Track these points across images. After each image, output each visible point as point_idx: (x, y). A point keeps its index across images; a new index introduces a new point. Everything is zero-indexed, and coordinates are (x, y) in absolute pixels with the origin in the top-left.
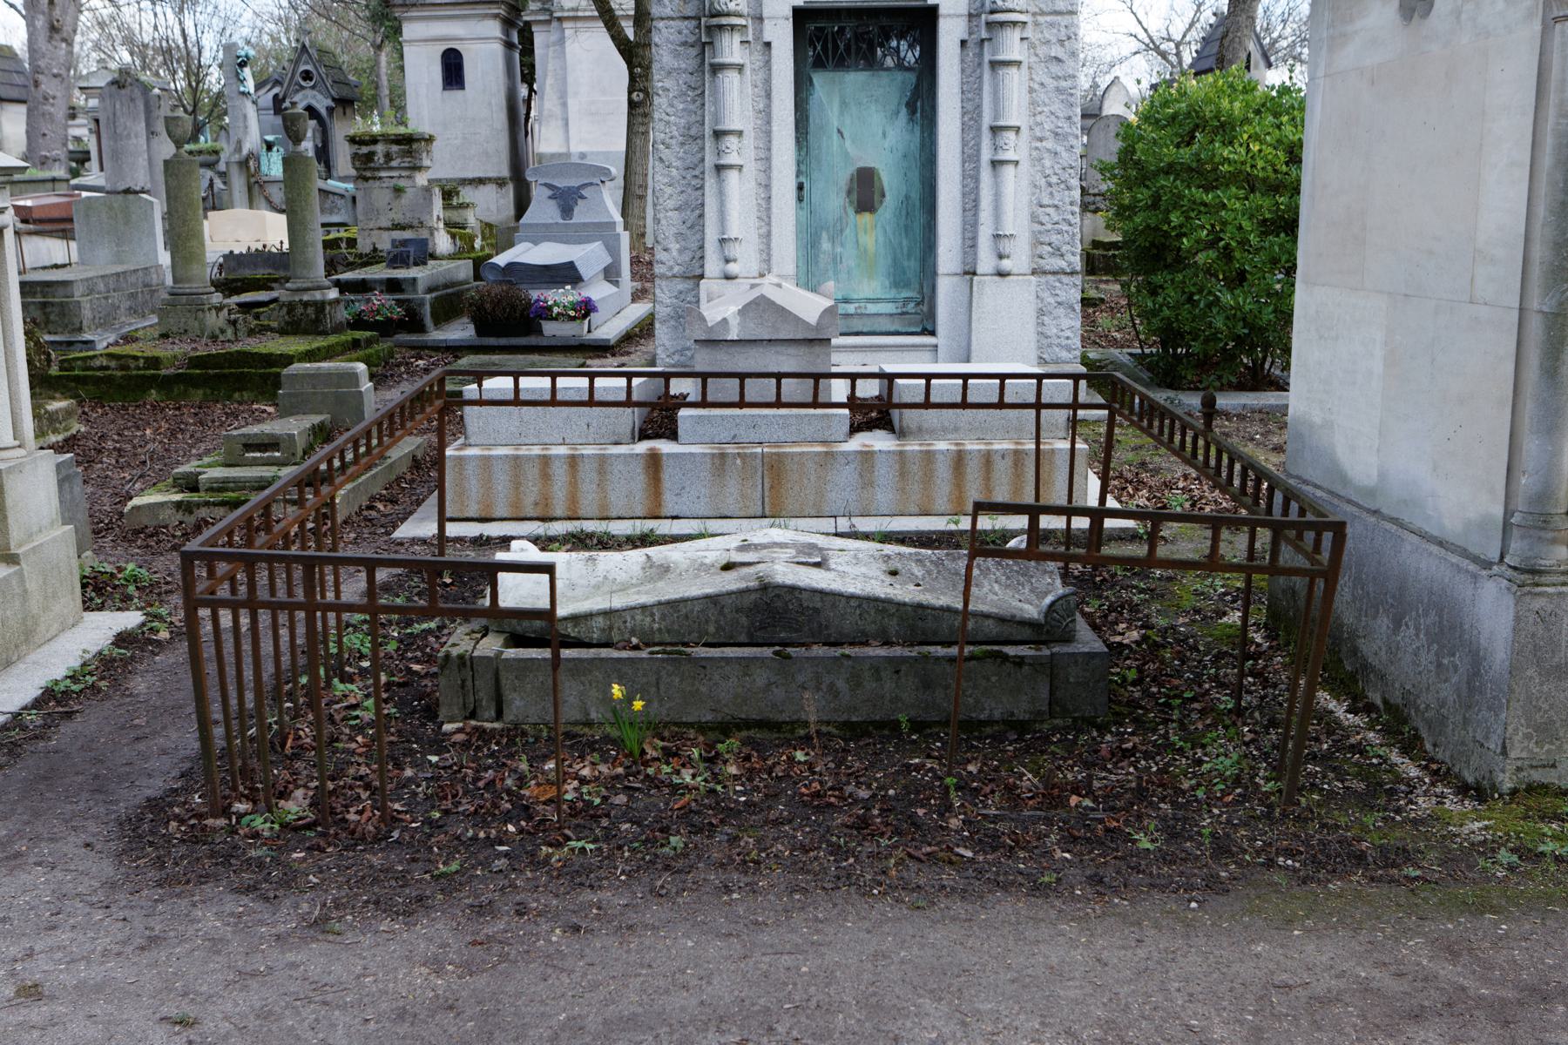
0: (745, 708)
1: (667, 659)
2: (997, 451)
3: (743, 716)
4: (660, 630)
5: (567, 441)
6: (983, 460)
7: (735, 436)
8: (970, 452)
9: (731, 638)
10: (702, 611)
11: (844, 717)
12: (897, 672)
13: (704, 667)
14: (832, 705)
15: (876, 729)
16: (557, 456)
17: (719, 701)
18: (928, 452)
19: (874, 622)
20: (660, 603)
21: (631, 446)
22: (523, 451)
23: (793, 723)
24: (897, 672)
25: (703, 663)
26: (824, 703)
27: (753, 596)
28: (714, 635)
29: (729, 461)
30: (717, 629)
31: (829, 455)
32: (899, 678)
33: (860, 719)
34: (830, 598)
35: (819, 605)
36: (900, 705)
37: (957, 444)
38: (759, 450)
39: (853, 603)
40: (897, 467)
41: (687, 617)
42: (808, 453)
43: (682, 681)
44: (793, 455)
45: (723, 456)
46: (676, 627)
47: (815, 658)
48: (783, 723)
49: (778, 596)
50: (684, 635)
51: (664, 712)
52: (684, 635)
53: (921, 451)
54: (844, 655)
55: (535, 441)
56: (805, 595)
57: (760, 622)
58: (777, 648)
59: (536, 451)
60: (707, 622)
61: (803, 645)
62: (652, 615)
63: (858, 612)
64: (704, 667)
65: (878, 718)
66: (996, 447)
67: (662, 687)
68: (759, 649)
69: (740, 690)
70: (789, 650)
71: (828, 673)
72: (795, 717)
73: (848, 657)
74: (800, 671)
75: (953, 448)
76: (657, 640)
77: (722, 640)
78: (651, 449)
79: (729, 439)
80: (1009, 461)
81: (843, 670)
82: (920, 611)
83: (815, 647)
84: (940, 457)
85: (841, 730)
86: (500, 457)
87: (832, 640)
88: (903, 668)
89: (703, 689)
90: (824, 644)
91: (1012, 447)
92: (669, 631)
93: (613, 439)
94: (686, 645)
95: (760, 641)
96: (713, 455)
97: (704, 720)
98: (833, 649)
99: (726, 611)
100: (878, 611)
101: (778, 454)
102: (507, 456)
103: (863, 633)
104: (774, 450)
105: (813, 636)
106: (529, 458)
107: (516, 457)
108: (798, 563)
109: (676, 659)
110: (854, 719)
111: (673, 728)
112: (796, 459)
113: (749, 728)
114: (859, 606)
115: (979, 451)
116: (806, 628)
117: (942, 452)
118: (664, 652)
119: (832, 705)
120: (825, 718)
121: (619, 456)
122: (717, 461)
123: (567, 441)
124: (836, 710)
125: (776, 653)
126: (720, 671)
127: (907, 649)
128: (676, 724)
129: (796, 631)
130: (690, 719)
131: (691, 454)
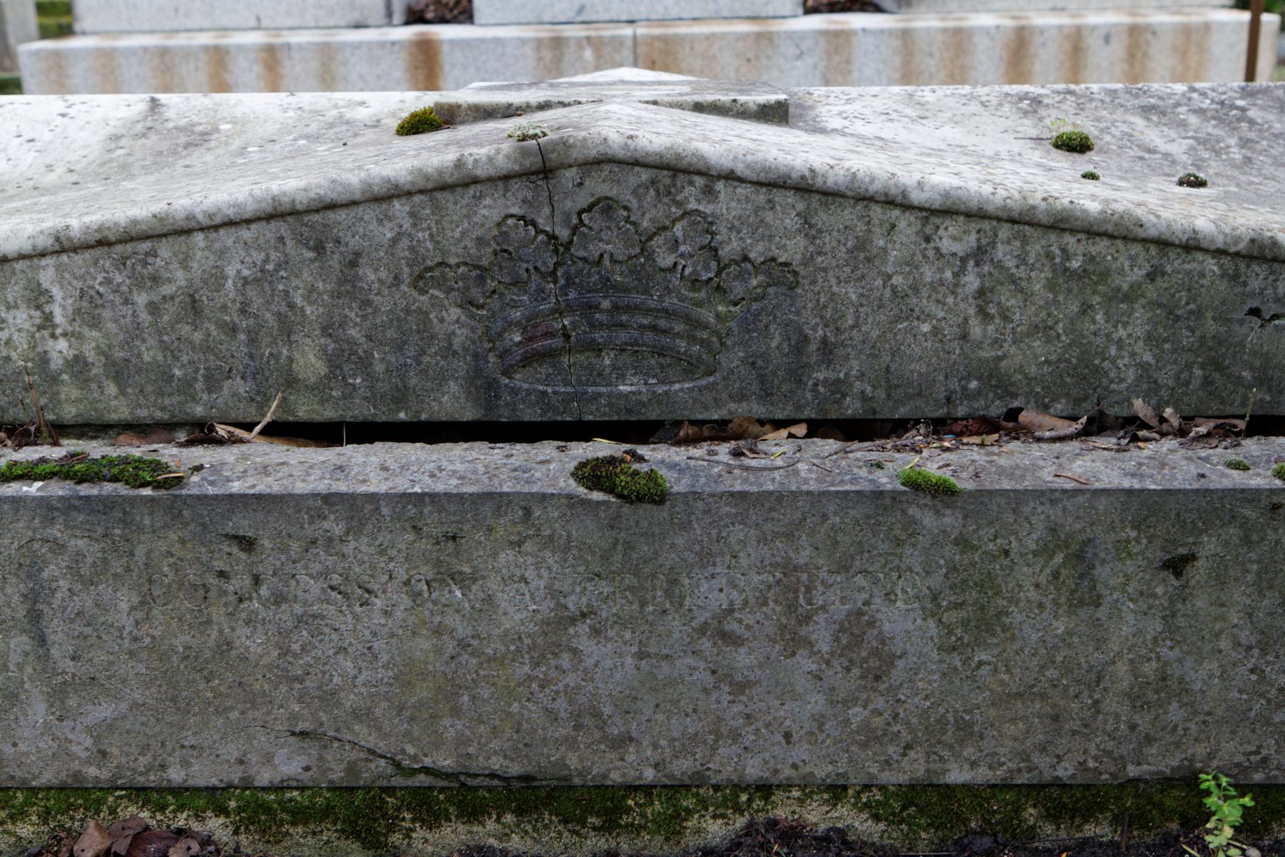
0: (451, 727)
1: (68, 506)
2: (1094, 28)
3: (446, 762)
4: (78, 365)
5: (265, 23)
6: (1067, 47)
7: (581, 9)
8: (1042, 31)
9: (400, 399)
10: (262, 278)
11: (914, 767)
12: (1177, 565)
13: (247, 544)
14: (857, 714)
15: (1054, 815)
16: (241, 48)
17: (329, 698)
18: (958, 32)
19: (1043, 329)
20: (63, 246)
21: (386, 30)
22: (180, 41)
23: (675, 789)
24: (1177, 565)
25: (242, 524)
26: (817, 703)
27: (492, 209)
28: (320, 389)
29: (570, 54)
30: (334, 363)
31: (765, 38)
32: (1182, 595)
33: (982, 775)
34: (849, 214)
35: (793, 249)
36: (1175, 712)
37: (1014, 18)
38: (628, 31)
39: (954, 238)
40: (897, 61)
41: (193, 307)
42: (723, 35)
43: (146, 603)
44: (692, 39)
45: (557, 43)
46: (149, 353)
47: (780, 498)
48: (633, 789)
49: (605, 206)
50: (186, 387)
51: (82, 744)
52: (186, 387)
53: (945, 31)
54: (917, 485)
55: (206, 23)
56: (728, 204)
57: (529, 327)
58: (602, 448)
59: (205, 39)
60: (287, 329)
61: (719, 431)
62: (38, 298)
63: (972, 281)
64: (247, 544)
65: (1065, 771)
66: (1093, 19)
67: (57, 630)
68: (520, 452)
69: (424, 644)
70: (656, 455)
71: (843, 567)
72: (683, 767)
73: (942, 492)
74: (706, 558)
75: (1008, 23)
76: (69, 413)
77: (361, 411)
78: (422, 34)
79: (570, 15)
80: (1118, 48)
81: (913, 558)
82: (1257, 277)
83: (777, 446)
84: (981, 42)
85: (894, 819)
86: (132, 52)
87: (851, 408)
88: (1209, 546)
89: (252, 642)
90: (817, 429)
91: (1125, 19)
92: (118, 372)
93: (355, 16)
94: (203, 434)
95: (530, 414)
96: (539, 42)
97: (264, 777)
98: (861, 452)
99: (368, 274)
100: (1063, 276)
101: (664, 39)
102: (145, 49)
103: (996, 381)
104: (656, 31)
105: (766, 395)
106: (187, 53)
107: (164, 52)
108: (699, 108)
109: (108, 504)
110: (957, 775)
111: (131, 811)
112: (700, 47)
113: (472, 812)
114: (979, 254)
115: (1060, 28)
116: (734, 358)
117: (986, 31)
118: (64, 471)
119: (857, 714)
120: (823, 771)
121: (357, 46)
122: (548, 55)
123: (265, 23)
124: (870, 738)
125: (592, 474)
126: (324, 559)
127: (1220, 453)
128: (139, 793)
129: (691, 368)
130: (203, 774)
131: (497, 41)
